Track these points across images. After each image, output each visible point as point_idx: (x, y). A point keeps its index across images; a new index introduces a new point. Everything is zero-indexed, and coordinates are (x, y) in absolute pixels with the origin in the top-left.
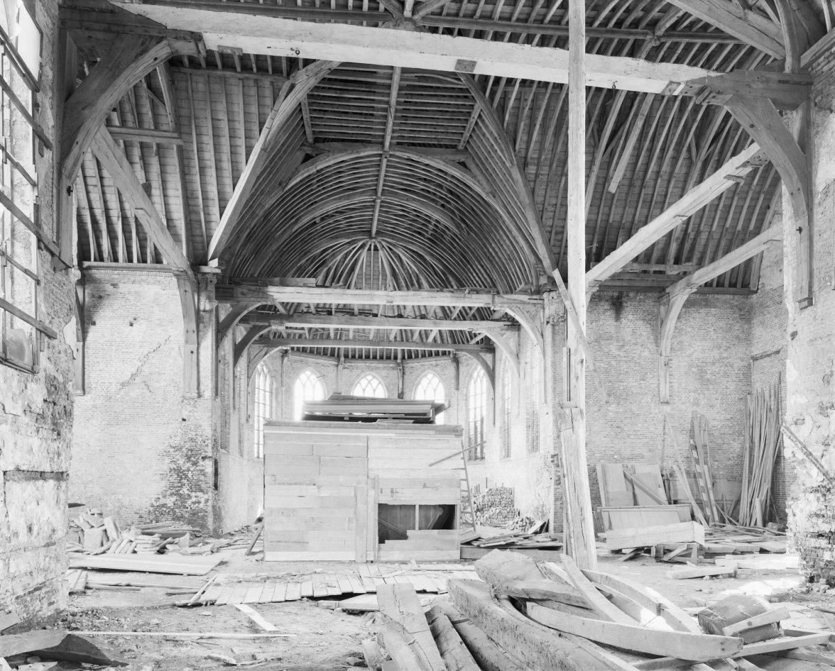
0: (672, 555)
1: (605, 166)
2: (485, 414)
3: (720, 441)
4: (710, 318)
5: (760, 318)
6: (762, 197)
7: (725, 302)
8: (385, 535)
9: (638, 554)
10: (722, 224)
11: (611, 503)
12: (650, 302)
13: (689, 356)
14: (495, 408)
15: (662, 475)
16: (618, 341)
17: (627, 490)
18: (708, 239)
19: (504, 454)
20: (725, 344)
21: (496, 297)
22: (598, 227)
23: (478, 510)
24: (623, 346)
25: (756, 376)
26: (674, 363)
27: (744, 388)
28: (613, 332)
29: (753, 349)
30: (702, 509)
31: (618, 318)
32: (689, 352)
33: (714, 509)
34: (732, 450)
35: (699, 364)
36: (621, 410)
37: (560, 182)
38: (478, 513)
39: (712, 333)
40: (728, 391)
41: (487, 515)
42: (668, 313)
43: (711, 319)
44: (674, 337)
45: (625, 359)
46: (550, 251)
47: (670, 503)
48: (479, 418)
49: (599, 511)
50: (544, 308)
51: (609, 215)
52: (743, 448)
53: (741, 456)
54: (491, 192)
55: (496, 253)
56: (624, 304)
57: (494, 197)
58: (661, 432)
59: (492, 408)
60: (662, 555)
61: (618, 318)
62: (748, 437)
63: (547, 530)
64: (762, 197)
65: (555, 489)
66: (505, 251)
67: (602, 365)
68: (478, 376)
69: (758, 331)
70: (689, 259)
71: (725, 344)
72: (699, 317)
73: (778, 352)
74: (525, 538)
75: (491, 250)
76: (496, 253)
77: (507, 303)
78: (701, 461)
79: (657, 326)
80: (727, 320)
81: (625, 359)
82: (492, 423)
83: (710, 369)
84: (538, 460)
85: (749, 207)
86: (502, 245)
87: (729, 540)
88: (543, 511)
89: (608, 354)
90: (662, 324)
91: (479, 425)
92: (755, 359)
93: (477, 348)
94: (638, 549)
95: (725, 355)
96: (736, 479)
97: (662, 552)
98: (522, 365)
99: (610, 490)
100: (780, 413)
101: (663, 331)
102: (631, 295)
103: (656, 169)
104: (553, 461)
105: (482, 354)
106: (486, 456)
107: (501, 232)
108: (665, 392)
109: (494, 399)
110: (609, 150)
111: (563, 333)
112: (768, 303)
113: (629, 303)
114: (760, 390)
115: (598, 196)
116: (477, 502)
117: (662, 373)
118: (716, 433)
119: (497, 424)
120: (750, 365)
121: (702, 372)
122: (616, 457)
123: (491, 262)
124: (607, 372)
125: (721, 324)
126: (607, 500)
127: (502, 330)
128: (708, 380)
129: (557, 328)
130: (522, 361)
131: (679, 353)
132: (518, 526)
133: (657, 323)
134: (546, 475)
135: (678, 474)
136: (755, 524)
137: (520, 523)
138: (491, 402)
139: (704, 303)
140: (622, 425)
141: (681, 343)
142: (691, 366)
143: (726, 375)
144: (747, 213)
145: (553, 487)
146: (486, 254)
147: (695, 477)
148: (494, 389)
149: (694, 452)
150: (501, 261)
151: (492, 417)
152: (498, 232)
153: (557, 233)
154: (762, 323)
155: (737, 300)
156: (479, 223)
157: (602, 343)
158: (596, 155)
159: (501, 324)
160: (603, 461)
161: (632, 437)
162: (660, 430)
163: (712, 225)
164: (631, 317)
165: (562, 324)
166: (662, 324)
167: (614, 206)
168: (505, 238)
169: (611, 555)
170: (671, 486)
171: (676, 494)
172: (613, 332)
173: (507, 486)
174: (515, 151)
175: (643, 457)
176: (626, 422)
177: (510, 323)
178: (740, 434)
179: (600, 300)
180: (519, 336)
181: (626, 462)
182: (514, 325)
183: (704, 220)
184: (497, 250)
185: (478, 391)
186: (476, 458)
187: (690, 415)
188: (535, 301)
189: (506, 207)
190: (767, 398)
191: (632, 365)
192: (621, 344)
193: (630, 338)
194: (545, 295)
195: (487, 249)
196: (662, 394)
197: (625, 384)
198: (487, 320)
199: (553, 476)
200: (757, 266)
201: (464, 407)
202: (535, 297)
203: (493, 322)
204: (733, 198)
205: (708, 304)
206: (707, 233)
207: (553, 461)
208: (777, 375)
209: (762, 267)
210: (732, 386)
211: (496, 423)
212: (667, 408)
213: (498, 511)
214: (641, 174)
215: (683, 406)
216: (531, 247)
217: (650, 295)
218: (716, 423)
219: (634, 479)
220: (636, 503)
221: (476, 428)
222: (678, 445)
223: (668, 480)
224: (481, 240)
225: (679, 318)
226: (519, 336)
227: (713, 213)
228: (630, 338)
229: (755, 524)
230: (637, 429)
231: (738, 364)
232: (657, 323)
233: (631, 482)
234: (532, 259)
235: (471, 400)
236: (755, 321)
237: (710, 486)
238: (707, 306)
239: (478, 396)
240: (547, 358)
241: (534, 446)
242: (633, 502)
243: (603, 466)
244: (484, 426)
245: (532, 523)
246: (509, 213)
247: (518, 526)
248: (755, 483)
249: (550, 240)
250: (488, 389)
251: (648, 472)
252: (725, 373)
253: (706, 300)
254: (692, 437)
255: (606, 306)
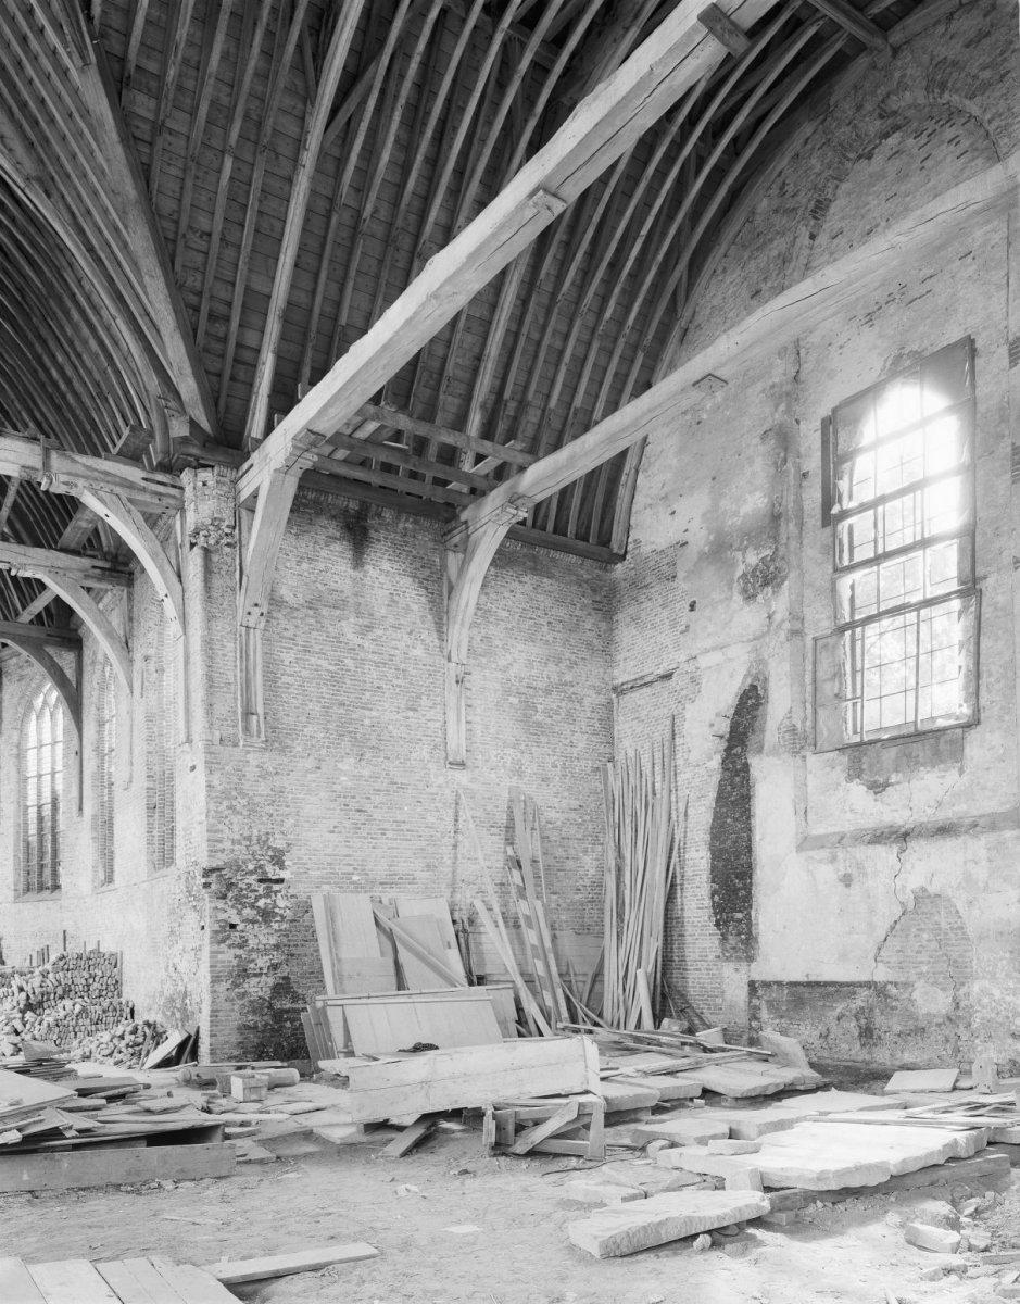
0: (537, 1135)
1: (330, 167)
2: (60, 787)
3: (560, 852)
4: (541, 598)
5: (631, 610)
6: (640, 358)
7: (568, 570)
8: (848, 886)
9: (431, 1130)
10: (566, 398)
11: (348, 985)
12: (424, 538)
13: (505, 669)
14: (81, 772)
15: (454, 922)
16: (359, 614)
17: (382, 954)
18: (540, 426)
19: (102, 876)
20: (567, 655)
21: (54, 455)
22: (314, 327)
23: (29, 1007)
24: (369, 628)
25: (623, 726)
26: (476, 679)
27: (601, 749)
28: (348, 592)
29: (616, 673)
30: (534, 993)
31: (358, 562)
32: (502, 662)
33: (559, 992)
34: (581, 871)
35: (524, 690)
36: (366, 773)
37: (219, 171)
38: (29, 1015)
39: (545, 629)
40: (575, 750)
41: (51, 1020)
42: (463, 567)
43: (545, 601)
44: (474, 625)
45: (375, 657)
46: (197, 357)
47: (471, 983)
48: (47, 797)
49: (319, 1004)
50: (182, 510)
51: (338, 305)
52: (601, 869)
53: (599, 885)
54: (39, 180)
55: (68, 382)
56: (372, 533)
57: (48, 195)
58: (451, 828)
59: (75, 772)
60: (511, 1136)
61: (358, 562)
62: (612, 845)
63: (194, 1055)
64: (640, 358)
65: (213, 954)
66: (89, 373)
67: (324, 663)
68: (45, 703)
69: (626, 635)
70: (511, 435)
71: (567, 655)
72: (521, 590)
73: (667, 676)
74: (111, 1099)
75: (55, 373)
76: (68, 382)
77: (86, 478)
78: (530, 891)
79: (441, 595)
80: (571, 608)
81: (375, 657)
82: (75, 808)
83: (542, 703)
84: (171, 884)
85: (616, 374)
86: (79, 356)
87: (629, 1070)
88: (184, 1009)
89: (338, 640)
90: (450, 593)
91: (47, 811)
92: (619, 691)
93: (36, 632)
94: (430, 1119)
95: (568, 677)
96: (589, 930)
97: (511, 1128)
98: (138, 664)
99: (345, 954)
100: (673, 798)
101: (453, 606)
102: (388, 515)
103: (443, 220)
104: (207, 885)
105: (50, 650)
106: (63, 881)
107: (76, 316)
108: (457, 741)
109: (79, 753)
110: (342, 118)
111: (231, 574)
112: (648, 580)
113: (382, 534)
114: (631, 753)
115: (314, 244)
116: (27, 988)
117: (452, 699)
118: (554, 836)
119: (88, 809)
120: (610, 703)
121: (528, 706)
122: (355, 878)
123: (58, 409)
124: (334, 680)
125: (562, 612)
126: (339, 978)
127: (87, 577)
128: (539, 724)
129: (215, 558)
130: (138, 656)
131: (484, 660)
132: (123, 1043)
133: (439, 590)
134: (192, 919)
135: (484, 917)
136: (639, 1025)
137: (129, 1038)
138: (73, 759)
139: (531, 564)
140: (368, 807)
141: (486, 639)
142: (508, 692)
143: (570, 718)
144: (612, 387)
145: (207, 950)
146: (43, 385)
147: (517, 926)
148: (80, 730)
149: (516, 873)
150: (82, 404)
151: (75, 793)
152: (67, 313)
153: (212, 317)
154: (635, 619)
155: (588, 569)
156: (20, 290)
157: (325, 612)
158: (310, 121)
159: (85, 562)
160: (326, 887)
161: (390, 834)
162: (449, 820)
163: (548, 396)
164: (386, 566)
165: (227, 550)
166: (450, 593)
167: (350, 284)
168: (86, 331)
169: (365, 1138)
170: (472, 946)
171: (482, 963)
172: (348, 592)
173: (106, 948)
174: (89, 18)
175: (413, 881)
176: (377, 799)
177: (107, 565)
178: (596, 841)
179: (319, 513)
180: (130, 598)
181: (378, 892)
182: (119, 566)
183: (536, 378)
184: (69, 371)
185: (47, 738)
186: (41, 888)
187: (506, 795)
188: (161, 489)
189: (81, 232)
190: (647, 770)
191: (390, 674)
192: (366, 622)
193: (384, 611)
194: (186, 477)
195: (47, 371)
196: (452, 744)
197: (374, 713)
198: (50, 547)
199: (207, 922)
200: (625, 506)
201: (13, 772)
202: (160, 477)
203: (62, 555)
204: (589, 344)
205: (536, 568)
206: (539, 412)
207: (207, 885)
208: (668, 722)
209: (634, 510)
210: (582, 743)
211: (85, 807)
212: (462, 777)
213: (78, 1008)
214: (412, 218)
215: (493, 775)
216: (149, 350)
217: (426, 523)
218: (552, 815)
219: (397, 931)
220: (401, 985)
221: (40, 819)
222: (482, 857)
223: (465, 931)
224: (31, 346)
225: (484, 586)
226: (130, 598)
227: (552, 370)
228: (384, 611)
229: (639, 1025)
230: (399, 818)
231: (591, 699)
232: (439, 590)
233: (390, 935)
234: (153, 383)
235: (32, 755)
236: (620, 616)
237: (548, 944)
238: (534, 571)
239: (46, 751)
240: (191, 631)
241: (163, 854)
242: (394, 980)
243: (328, 899)
244: (61, 817)
245: (158, 1037)
246: (91, 249)
247: (123, 1043)
248: (630, 936)
249: (195, 331)
250: (66, 731)
251: (425, 914)
252: (569, 714)
253: (534, 558)
254: (510, 841)
255: (333, 529)
